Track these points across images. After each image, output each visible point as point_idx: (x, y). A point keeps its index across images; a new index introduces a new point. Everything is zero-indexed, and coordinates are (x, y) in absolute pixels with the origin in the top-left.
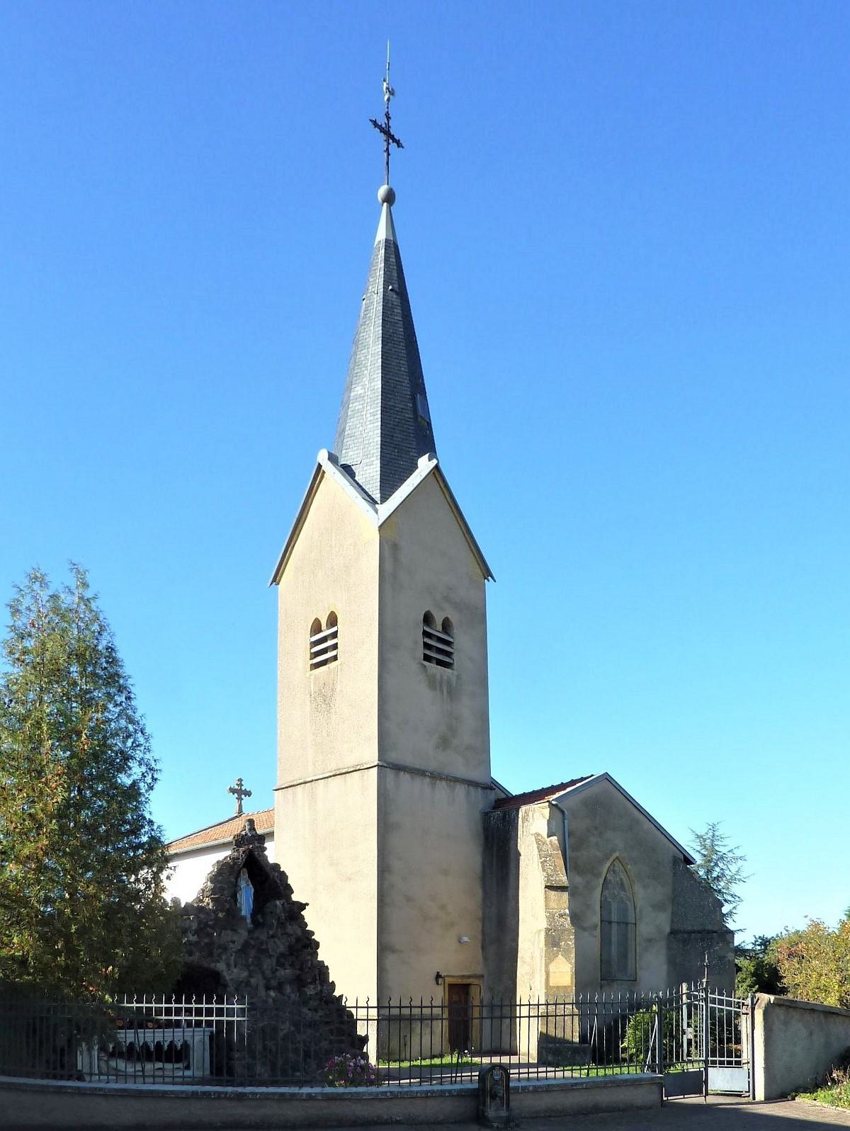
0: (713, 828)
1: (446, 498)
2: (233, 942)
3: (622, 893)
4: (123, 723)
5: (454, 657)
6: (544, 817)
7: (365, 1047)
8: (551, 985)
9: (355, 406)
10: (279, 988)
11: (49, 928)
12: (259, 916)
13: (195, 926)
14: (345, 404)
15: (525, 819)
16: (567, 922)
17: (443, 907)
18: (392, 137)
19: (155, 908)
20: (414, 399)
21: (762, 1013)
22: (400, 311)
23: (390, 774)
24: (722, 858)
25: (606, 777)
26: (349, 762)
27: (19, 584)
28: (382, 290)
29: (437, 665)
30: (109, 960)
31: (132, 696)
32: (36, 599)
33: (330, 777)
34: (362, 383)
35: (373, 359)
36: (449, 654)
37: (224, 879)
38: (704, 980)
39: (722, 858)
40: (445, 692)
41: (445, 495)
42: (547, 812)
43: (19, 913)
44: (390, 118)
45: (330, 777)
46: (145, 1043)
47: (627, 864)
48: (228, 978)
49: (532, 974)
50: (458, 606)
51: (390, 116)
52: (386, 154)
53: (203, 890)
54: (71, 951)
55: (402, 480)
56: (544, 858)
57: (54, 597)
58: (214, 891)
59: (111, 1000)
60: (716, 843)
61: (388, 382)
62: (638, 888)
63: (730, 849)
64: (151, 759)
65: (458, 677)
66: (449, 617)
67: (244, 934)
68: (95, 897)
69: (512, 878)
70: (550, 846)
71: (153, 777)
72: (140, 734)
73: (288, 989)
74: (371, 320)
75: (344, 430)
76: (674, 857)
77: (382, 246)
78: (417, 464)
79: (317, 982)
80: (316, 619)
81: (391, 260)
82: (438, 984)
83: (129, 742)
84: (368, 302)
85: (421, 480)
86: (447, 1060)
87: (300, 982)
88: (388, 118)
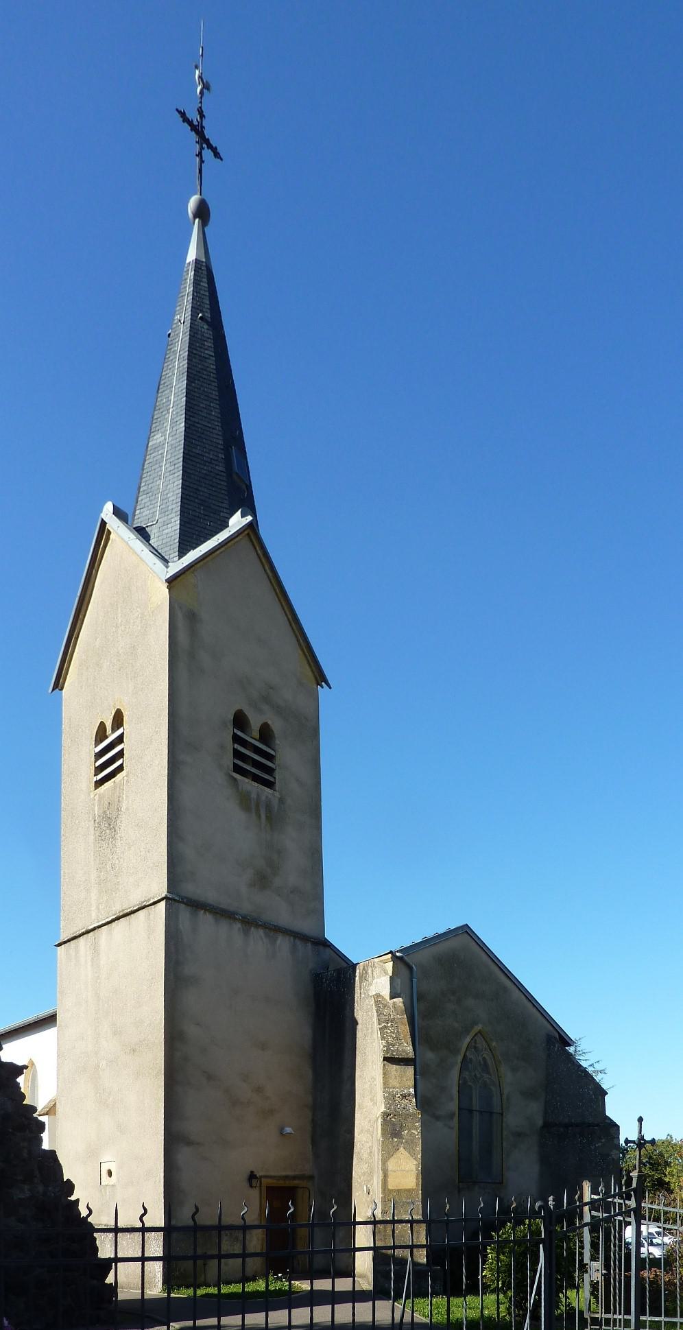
1: (265, 571)
3: (486, 1076)
5: (277, 774)
6: (386, 973)
7: (112, 1273)
8: (390, 1187)
16: (411, 1106)
23: (184, 913)
29: (252, 780)
36: (270, 771)
40: (263, 816)
41: (255, 548)
44: (204, 116)
49: (371, 1173)
50: (279, 710)
56: (385, 1022)
61: (194, 426)
62: (504, 1069)
65: (282, 801)
66: (270, 722)
70: (392, 1009)
76: (548, 1035)
80: (102, 723)
82: (251, 1186)
86: (260, 1285)
88: (202, 116)
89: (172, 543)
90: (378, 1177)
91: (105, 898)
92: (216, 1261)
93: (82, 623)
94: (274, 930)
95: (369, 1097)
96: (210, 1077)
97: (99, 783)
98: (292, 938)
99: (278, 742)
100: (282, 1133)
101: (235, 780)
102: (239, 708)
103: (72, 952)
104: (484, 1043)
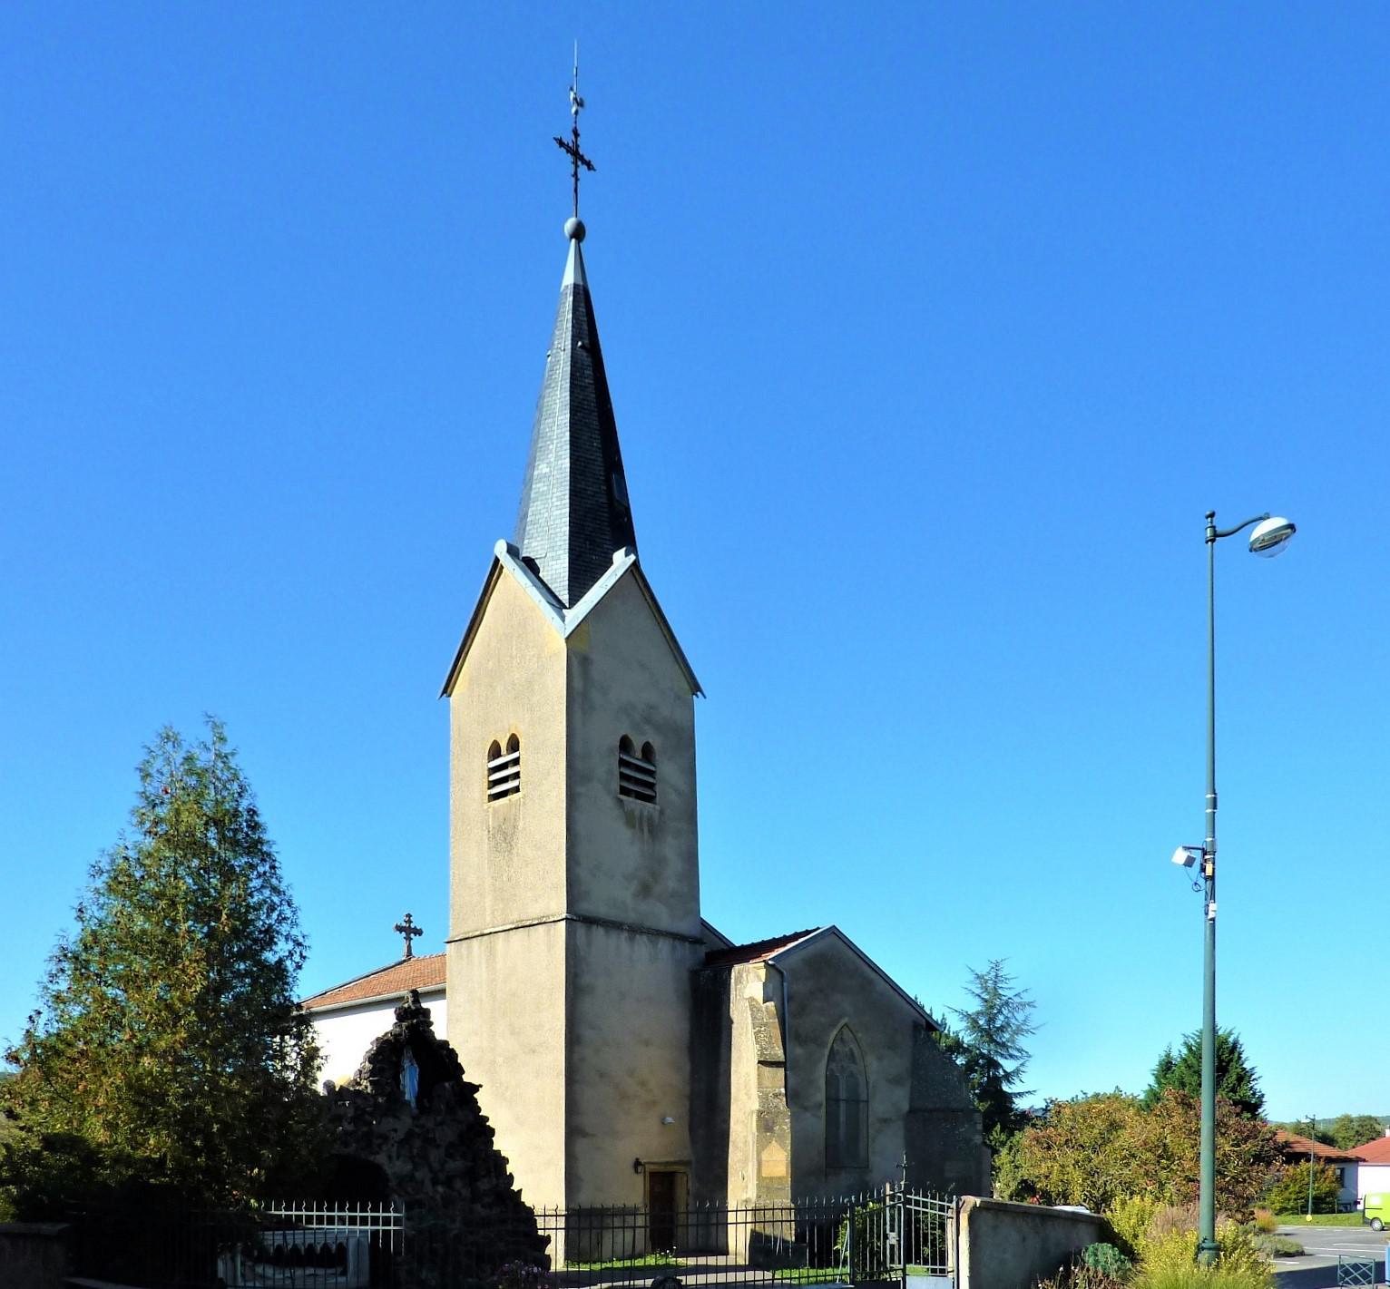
0: (996, 966)
1: (646, 600)
2: (395, 1130)
4: (267, 892)
5: (657, 788)
6: (758, 977)
8: (764, 1175)
9: (538, 487)
10: (448, 1182)
11: (187, 1124)
12: (425, 1100)
13: (351, 1113)
14: (527, 482)
15: (739, 981)
17: (643, 1084)
18: (582, 158)
19: (303, 1094)
20: (608, 482)
21: (967, 1217)
22: (591, 373)
23: (581, 930)
24: (1007, 1003)
25: (833, 931)
26: (534, 912)
27: (148, 745)
28: (570, 346)
30: (255, 1161)
31: (277, 864)
32: (168, 761)
33: (512, 929)
34: (548, 461)
35: (559, 431)
36: (651, 786)
37: (385, 1056)
38: (902, 1183)
39: (1007, 1003)
42: (763, 973)
43: (155, 1112)
45: (512, 929)
46: (295, 1246)
47: (857, 1032)
48: (389, 1171)
49: (745, 1162)
51: (579, 132)
52: (573, 179)
53: (360, 1072)
54: (211, 1149)
55: (595, 579)
57: (189, 759)
58: (372, 1073)
59: (256, 1205)
60: (1000, 985)
63: (1016, 993)
64: (299, 934)
65: (662, 812)
66: (651, 741)
67: (407, 1121)
68: (239, 1093)
69: (723, 1050)
70: (765, 1013)
71: (301, 954)
72: (286, 907)
73: (458, 1184)
74: (557, 382)
75: (526, 515)
77: (570, 291)
78: (612, 559)
79: (493, 1174)
81: (580, 309)
82: (636, 1172)
83: (275, 915)
84: (553, 360)
85: (606, 590)
87: (471, 1176)
88: (576, 134)
89: (562, 580)
90: (753, 1165)
91: (501, 906)
92: (715, 1227)
93: (472, 642)
94: (655, 933)
95: (744, 1092)
96: (602, 1075)
98: (671, 940)
99: (658, 757)
100: (663, 1123)
101: (621, 801)
103: (464, 952)
104: (851, 1035)
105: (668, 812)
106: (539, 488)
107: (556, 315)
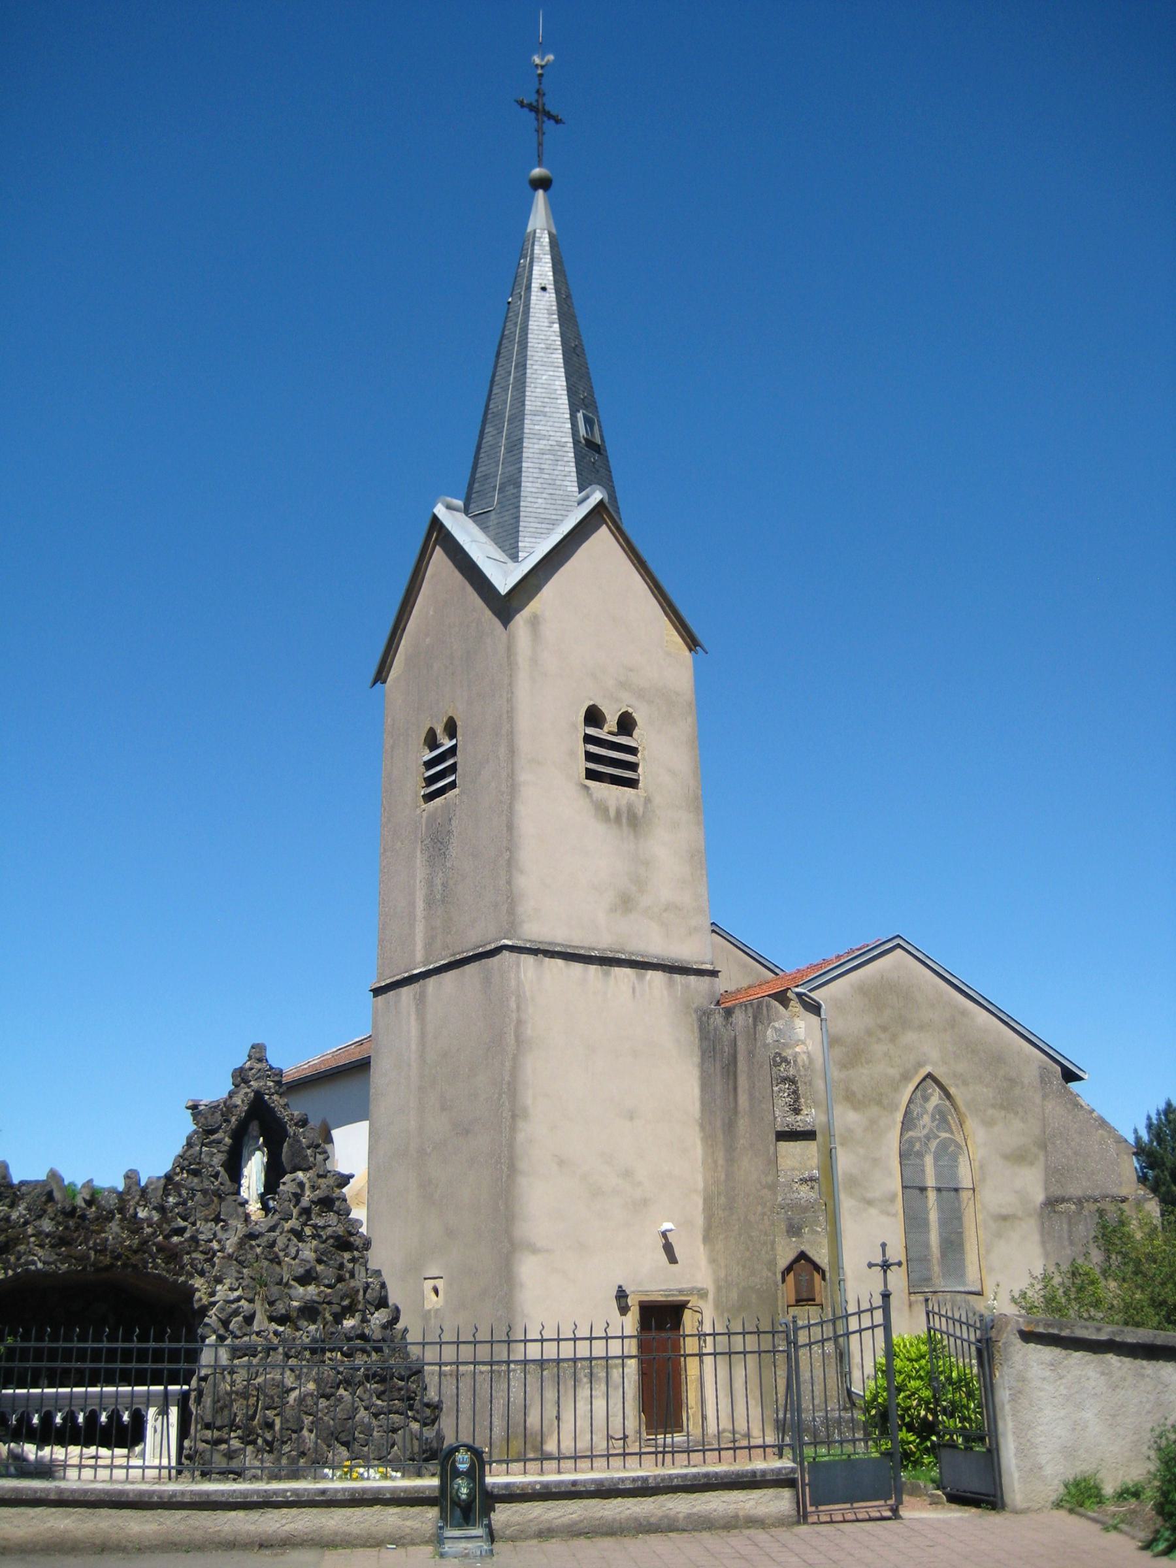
36: (633, 767)
50: (640, 694)
65: (648, 800)
96: (561, 1163)
97: (429, 797)
101: (586, 788)
102: (591, 703)
105: (657, 800)
106: (514, 488)
107: (520, 282)
